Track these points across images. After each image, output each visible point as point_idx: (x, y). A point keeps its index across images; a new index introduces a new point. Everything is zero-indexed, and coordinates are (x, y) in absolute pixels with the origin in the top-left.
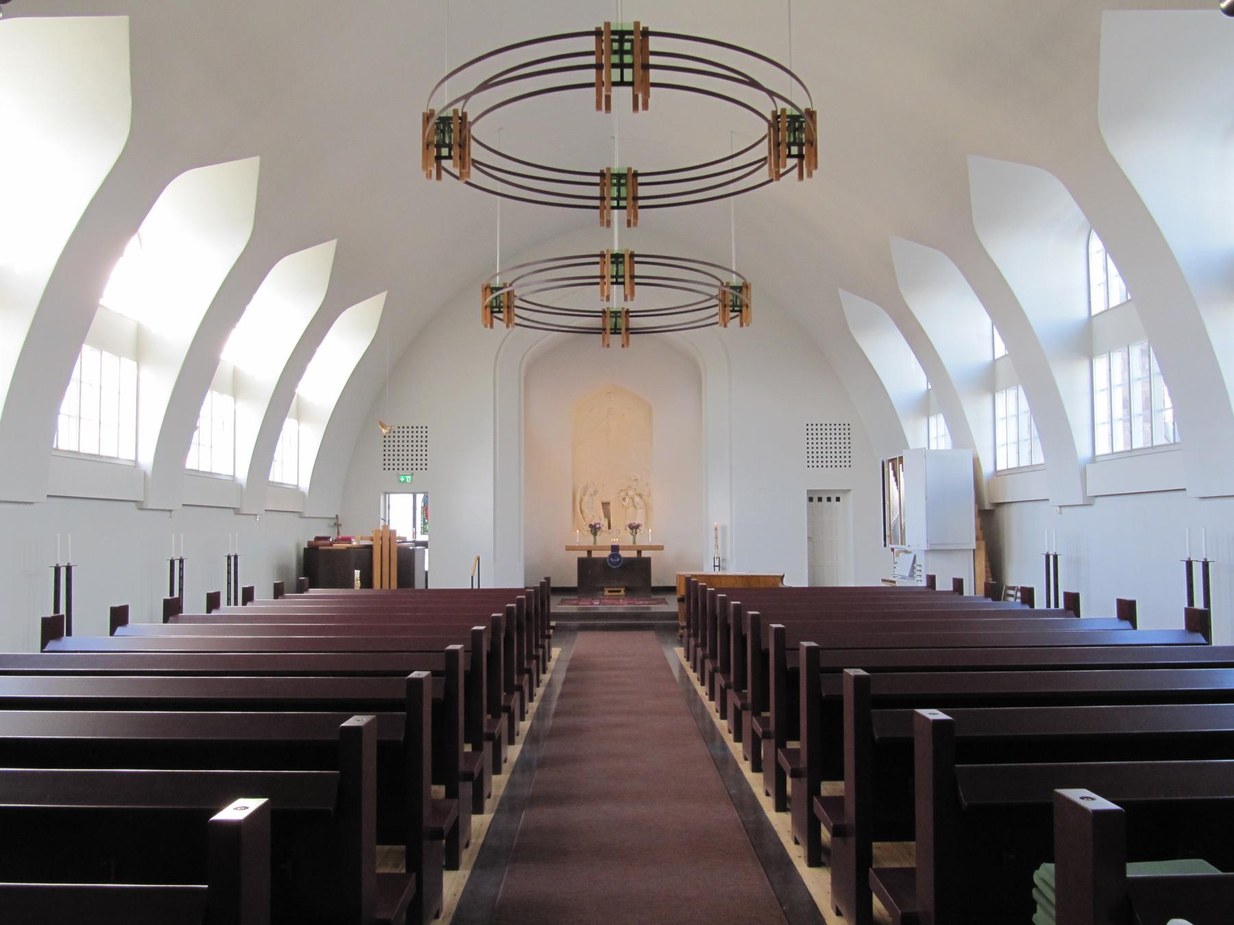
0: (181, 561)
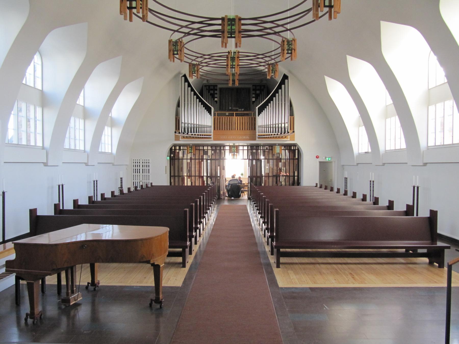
0: (97, 181)
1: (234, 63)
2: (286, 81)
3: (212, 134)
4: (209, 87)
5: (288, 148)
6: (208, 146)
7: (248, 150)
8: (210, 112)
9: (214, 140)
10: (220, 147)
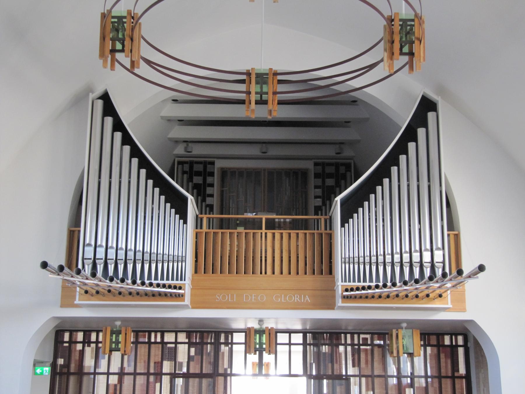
1: (265, 89)
2: (431, 116)
3: (187, 283)
4: (191, 167)
5: (433, 340)
6: (176, 332)
7: (305, 344)
8: (179, 206)
9: (195, 305)
10: (217, 334)
